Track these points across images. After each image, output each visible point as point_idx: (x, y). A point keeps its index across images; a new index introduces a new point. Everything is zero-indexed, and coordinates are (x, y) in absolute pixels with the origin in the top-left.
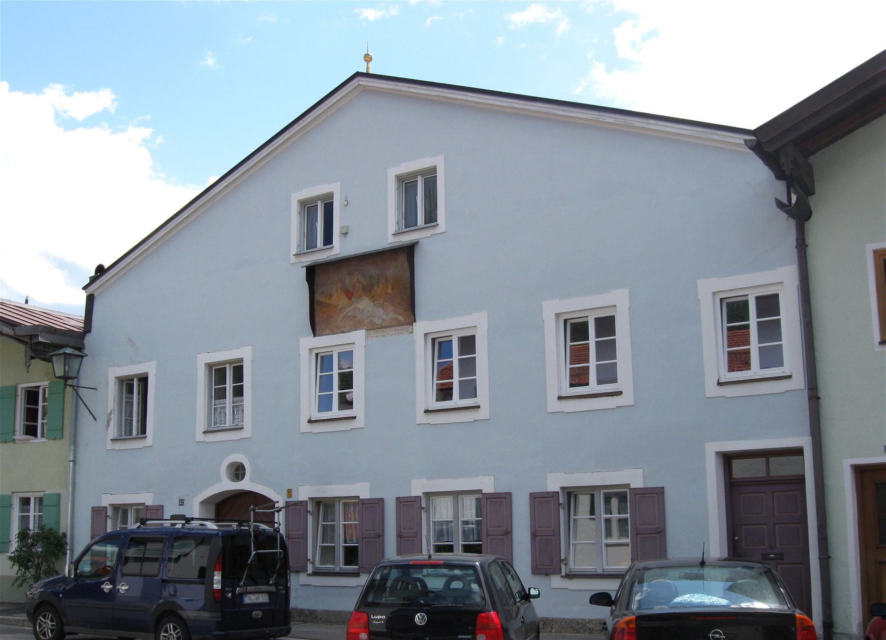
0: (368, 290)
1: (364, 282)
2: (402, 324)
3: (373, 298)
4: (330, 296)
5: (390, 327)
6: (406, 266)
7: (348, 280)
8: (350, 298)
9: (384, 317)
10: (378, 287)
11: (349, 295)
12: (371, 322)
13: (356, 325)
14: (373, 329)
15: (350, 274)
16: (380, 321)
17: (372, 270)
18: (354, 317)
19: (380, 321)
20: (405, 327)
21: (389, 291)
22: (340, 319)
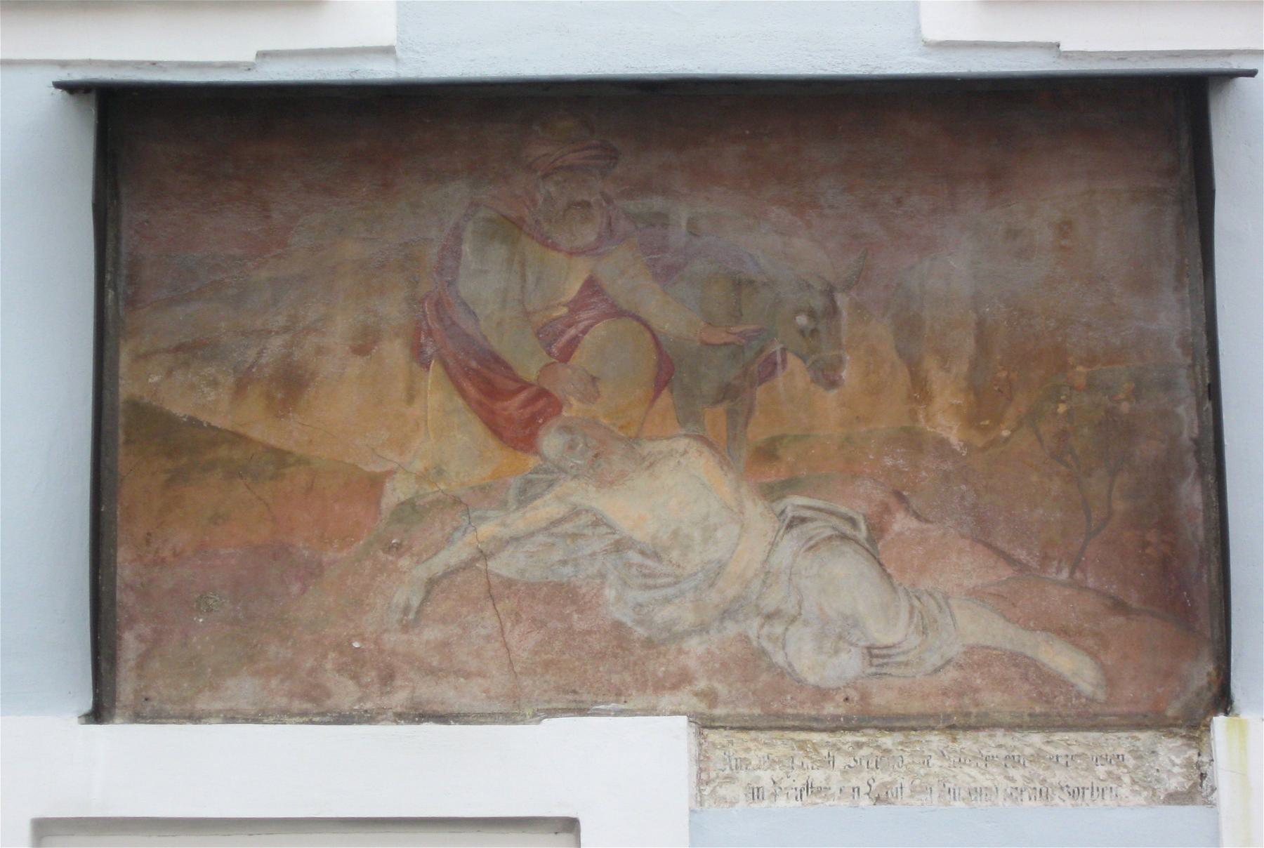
0: (715, 386)
1: (672, 315)
2: (1089, 719)
3: (770, 465)
4: (291, 385)
5: (955, 725)
6: (1200, 286)
7: (486, 286)
8: (521, 436)
9: (892, 631)
10: (827, 376)
11: (509, 404)
12: (751, 663)
13: (589, 667)
14: (775, 723)
15: (509, 229)
16: (849, 664)
17: (776, 241)
18: (564, 595)
19: (849, 664)
20: (1119, 742)
21: (946, 424)
22: (406, 594)
